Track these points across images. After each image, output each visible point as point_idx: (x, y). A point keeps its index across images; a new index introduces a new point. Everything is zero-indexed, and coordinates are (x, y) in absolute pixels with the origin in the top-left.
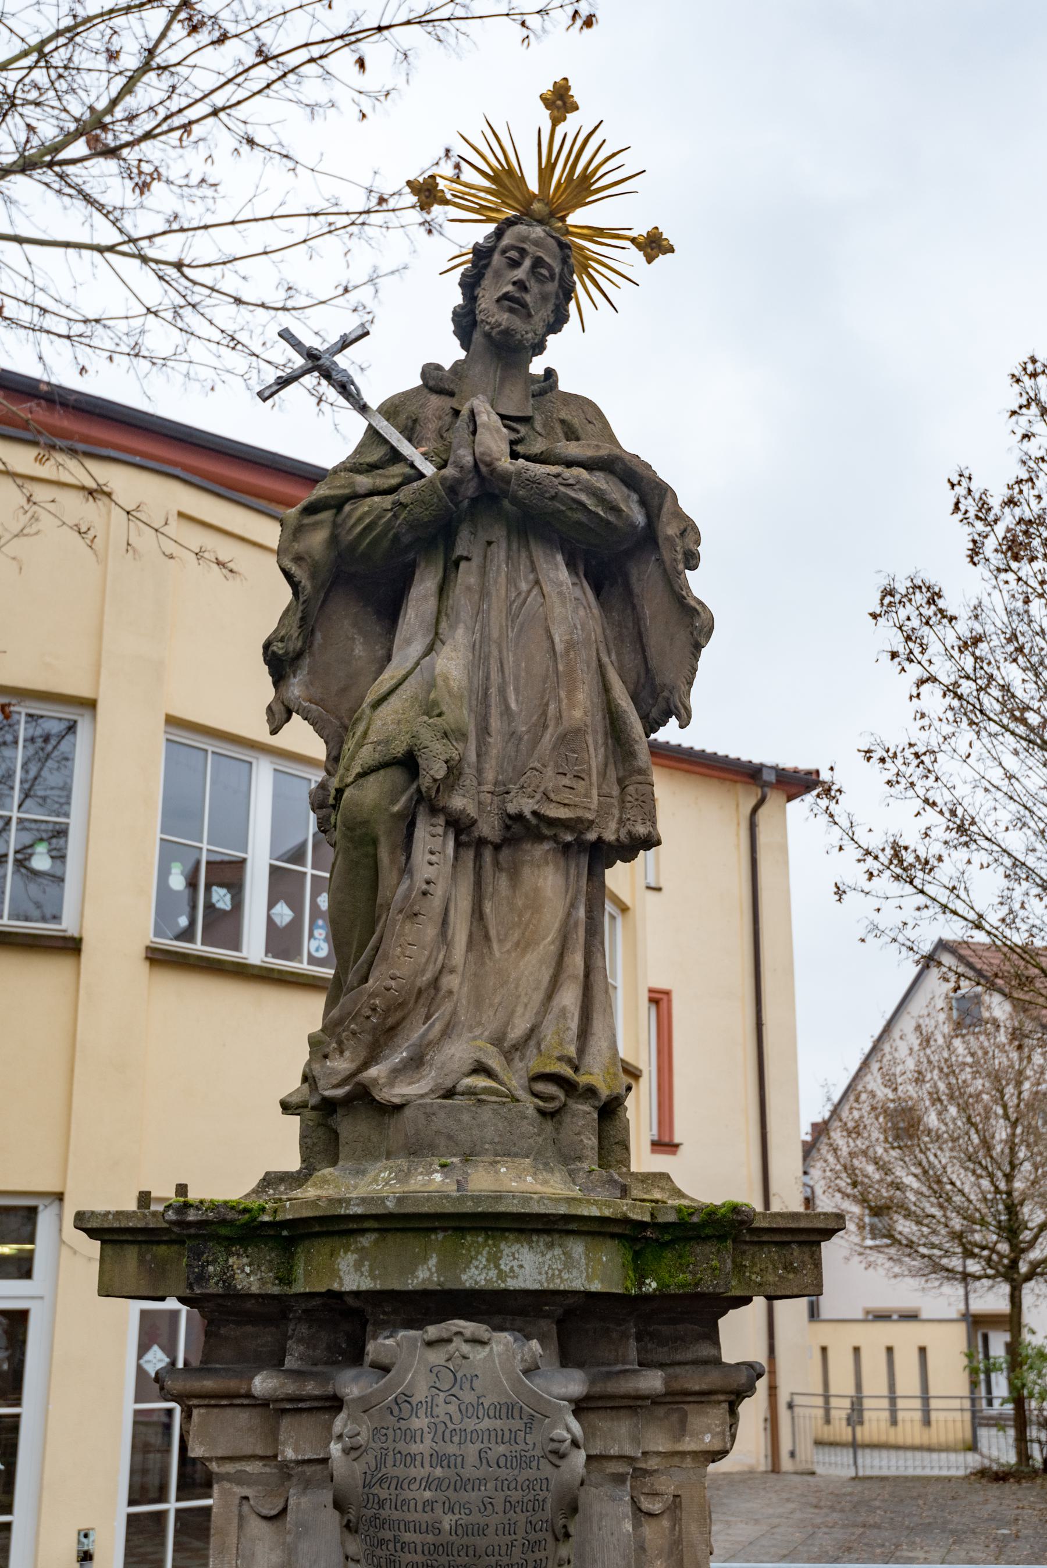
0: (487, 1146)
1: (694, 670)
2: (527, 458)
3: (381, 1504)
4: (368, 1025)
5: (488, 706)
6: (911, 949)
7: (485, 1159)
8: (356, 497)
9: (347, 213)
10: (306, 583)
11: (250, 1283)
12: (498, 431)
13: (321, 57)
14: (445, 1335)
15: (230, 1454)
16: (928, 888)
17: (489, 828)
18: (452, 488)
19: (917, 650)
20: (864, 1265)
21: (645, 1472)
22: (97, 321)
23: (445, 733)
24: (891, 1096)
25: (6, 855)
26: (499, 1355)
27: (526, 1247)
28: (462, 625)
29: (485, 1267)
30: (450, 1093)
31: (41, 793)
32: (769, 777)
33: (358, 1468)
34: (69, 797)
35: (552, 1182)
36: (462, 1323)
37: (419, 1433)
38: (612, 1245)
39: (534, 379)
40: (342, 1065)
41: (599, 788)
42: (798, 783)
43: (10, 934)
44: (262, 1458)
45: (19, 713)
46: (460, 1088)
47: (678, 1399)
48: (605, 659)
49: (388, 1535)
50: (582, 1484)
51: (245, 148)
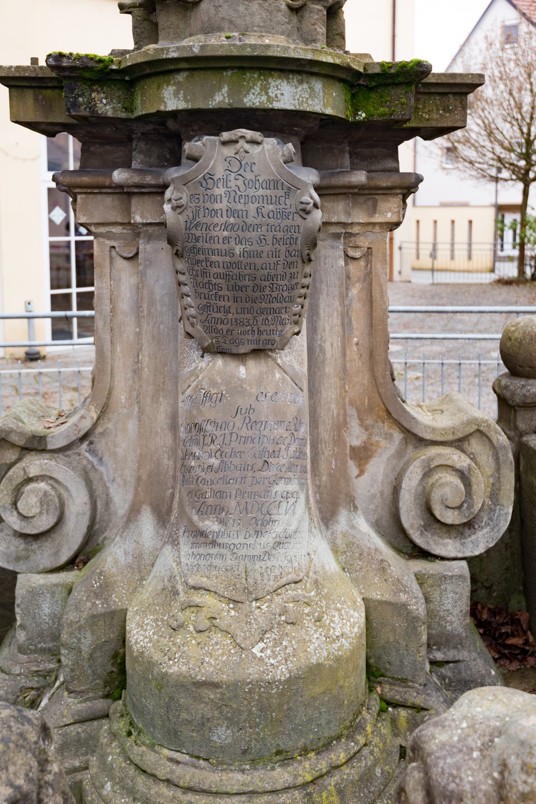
3: (197, 240)
14: (234, 138)
15: (101, 221)
21: (351, 235)
26: (268, 151)
27: (286, 82)
29: (259, 94)
33: (182, 219)
37: (219, 197)
38: (339, 86)
44: (121, 224)
49: (202, 257)
50: (319, 230)
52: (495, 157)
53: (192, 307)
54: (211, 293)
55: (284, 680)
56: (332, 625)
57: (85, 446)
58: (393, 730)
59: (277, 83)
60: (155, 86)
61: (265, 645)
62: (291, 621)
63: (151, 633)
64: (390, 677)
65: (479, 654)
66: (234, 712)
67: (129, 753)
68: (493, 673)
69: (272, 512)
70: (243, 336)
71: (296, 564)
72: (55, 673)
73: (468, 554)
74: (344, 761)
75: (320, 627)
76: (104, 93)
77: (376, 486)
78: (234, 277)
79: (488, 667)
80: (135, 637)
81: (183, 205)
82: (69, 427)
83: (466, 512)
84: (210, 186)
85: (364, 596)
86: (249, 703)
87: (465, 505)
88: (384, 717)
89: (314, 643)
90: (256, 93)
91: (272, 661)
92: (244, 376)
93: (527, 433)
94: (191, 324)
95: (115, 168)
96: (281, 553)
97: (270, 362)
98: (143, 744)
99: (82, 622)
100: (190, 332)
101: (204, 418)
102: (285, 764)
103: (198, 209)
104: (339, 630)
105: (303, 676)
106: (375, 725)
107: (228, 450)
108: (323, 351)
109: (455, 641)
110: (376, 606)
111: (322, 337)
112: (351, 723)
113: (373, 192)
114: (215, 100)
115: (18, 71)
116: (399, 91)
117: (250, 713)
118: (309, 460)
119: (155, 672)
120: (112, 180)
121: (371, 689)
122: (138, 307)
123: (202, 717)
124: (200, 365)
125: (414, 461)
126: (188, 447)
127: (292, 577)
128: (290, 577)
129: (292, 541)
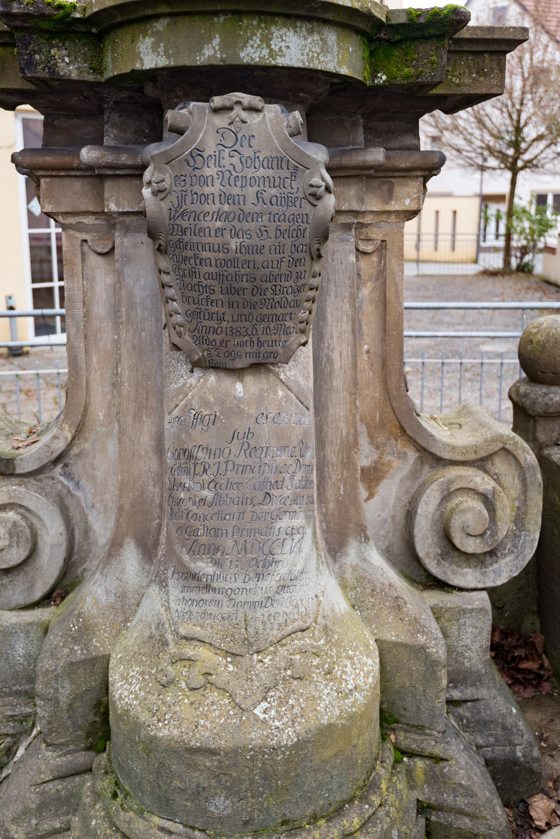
14: (227, 104)
15: (70, 210)
21: (361, 225)
26: (270, 120)
27: (292, 31)
29: (259, 46)
33: (165, 206)
36: (240, 94)
37: (210, 179)
44: (93, 213)
47: (389, 174)
49: (190, 253)
50: (332, 220)
52: (484, 145)
53: (179, 314)
54: (202, 297)
55: (291, 745)
56: (344, 677)
57: (58, 469)
58: (409, 783)
59: (281, 33)
60: (129, 38)
61: (268, 705)
62: (298, 676)
63: (137, 688)
64: (404, 724)
65: (498, 691)
66: (234, 781)
67: (115, 819)
68: (514, 711)
69: (275, 552)
70: (239, 348)
71: (302, 610)
72: (32, 718)
73: (490, 584)
74: (357, 827)
75: (331, 680)
76: (66, 49)
77: (387, 510)
78: (229, 278)
79: (508, 705)
80: (119, 692)
81: (166, 189)
82: (40, 448)
83: (489, 540)
84: (199, 165)
85: (377, 637)
86: (251, 771)
87: (489, 532)
88: (399, 770)
89: (325, 700)
90: (256, 45)
91: (277, 723)
92: (241, 395)
93: (547, 446)
94: (178, 333)
95: (83, 145)
96: (286, 598)
97: (272, 378)
98: (131, 808)
99: (59, 671)
100: (176, 343)
101: (195, 444)
102: (292, 834)
103: (184, 193)
104: (352, 682)
105: (313, 739)
106: (390, 780)
107: (222, 481)
108: (330, 361)
109: (473, 678)
110: (390, 648)
111: (329, 345)
112: (364, 782)
113: (389, 174)
114: (204, 55)
116: (428, 47)
117: (252, 781)
118: (315, 487)
119: (142, 735)
120: (80, 160)
121: (384, 737)
122: (115, 311)
123: (198, 786)
124: (189, 381)
125: (432, 483)
126: (176, 476)
127: (299, 624)
128: (296, 624)
129: (298, 583)
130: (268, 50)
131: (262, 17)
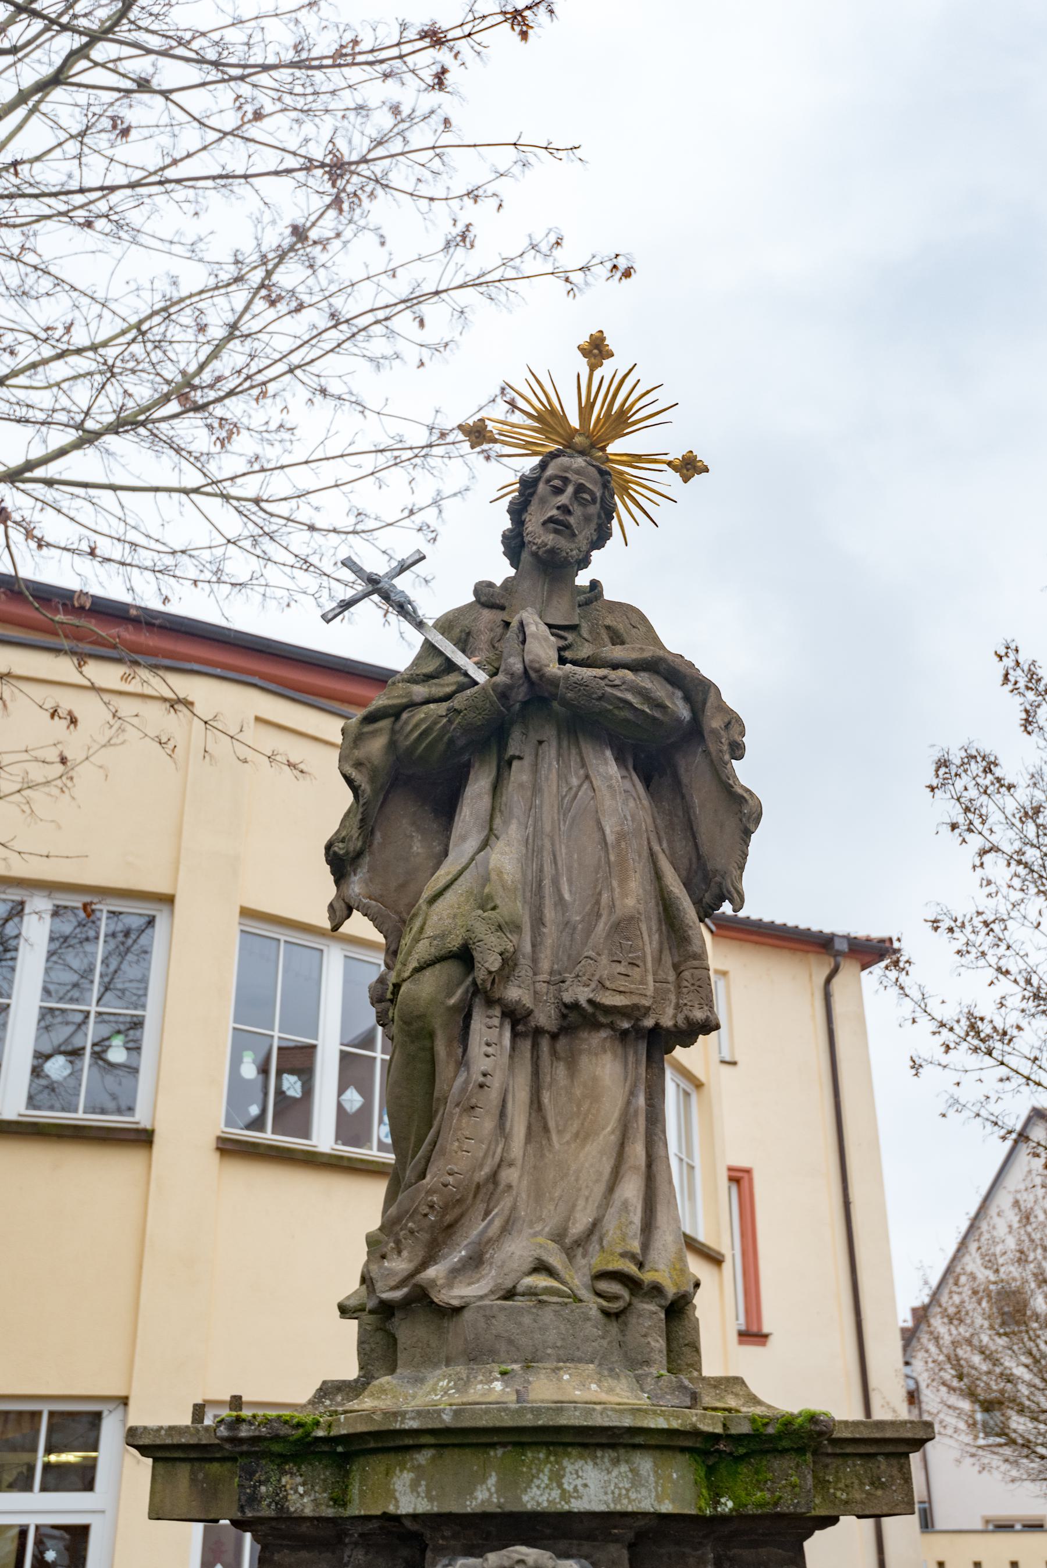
0: (549, 1351)
1: (745, 855)
2: (575, 663)
4: (425, 1223)
5: (542, 898)
6: (996, 1124)
7: (547, 1365)
8: (412, 705)
9: (411, 448)
10: (366, 786)
11: (303, 1505)
12: (546, 639)
13: (387, 319)
16: (1007, 1059)
17: (545, 1017)
18: (504, 694)
19: (977, 822)
20: (977, 1468)
22: (183, 552)
23: (500, 926)
24: (993, 1277)
25: (83, 1048)
27: (590, 1463)
28: (515, 821)
29: (547, 1486)
30: (510, 1294)
31: (119, 986)
32: (842, 946)
34: (146, 989)
35: (618, 1390)
38: (683, 1459)
39: (580, 590)
40: (400, 1265)
41: (655, 974)
42: (873, 952)
43: (84, 1127)
45: (101, 911)
46: (520, 1289)
48: (656, 848)
51: (318, 398)
59: (576, 1467)
76: (301, 1475)
90: (543, 1485)
114: (476, 1498)
115: (171, 1435)
130: (559, 1491)
131: (551, 1448)
